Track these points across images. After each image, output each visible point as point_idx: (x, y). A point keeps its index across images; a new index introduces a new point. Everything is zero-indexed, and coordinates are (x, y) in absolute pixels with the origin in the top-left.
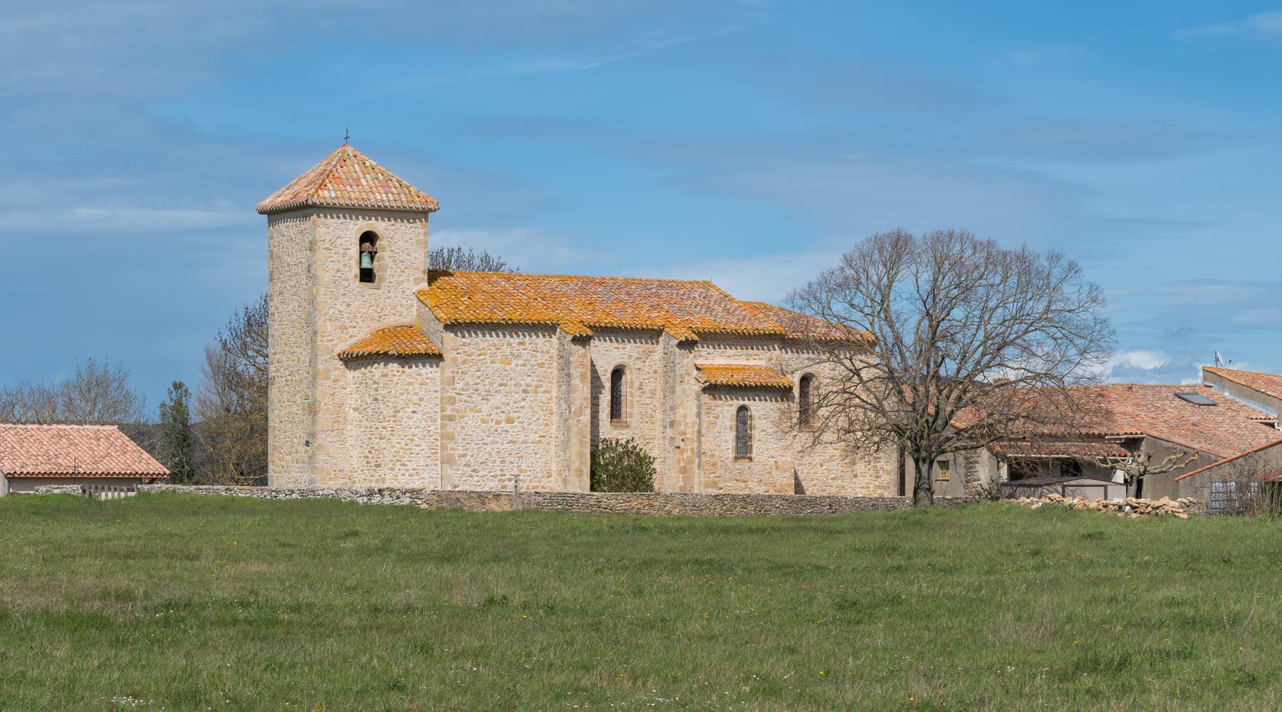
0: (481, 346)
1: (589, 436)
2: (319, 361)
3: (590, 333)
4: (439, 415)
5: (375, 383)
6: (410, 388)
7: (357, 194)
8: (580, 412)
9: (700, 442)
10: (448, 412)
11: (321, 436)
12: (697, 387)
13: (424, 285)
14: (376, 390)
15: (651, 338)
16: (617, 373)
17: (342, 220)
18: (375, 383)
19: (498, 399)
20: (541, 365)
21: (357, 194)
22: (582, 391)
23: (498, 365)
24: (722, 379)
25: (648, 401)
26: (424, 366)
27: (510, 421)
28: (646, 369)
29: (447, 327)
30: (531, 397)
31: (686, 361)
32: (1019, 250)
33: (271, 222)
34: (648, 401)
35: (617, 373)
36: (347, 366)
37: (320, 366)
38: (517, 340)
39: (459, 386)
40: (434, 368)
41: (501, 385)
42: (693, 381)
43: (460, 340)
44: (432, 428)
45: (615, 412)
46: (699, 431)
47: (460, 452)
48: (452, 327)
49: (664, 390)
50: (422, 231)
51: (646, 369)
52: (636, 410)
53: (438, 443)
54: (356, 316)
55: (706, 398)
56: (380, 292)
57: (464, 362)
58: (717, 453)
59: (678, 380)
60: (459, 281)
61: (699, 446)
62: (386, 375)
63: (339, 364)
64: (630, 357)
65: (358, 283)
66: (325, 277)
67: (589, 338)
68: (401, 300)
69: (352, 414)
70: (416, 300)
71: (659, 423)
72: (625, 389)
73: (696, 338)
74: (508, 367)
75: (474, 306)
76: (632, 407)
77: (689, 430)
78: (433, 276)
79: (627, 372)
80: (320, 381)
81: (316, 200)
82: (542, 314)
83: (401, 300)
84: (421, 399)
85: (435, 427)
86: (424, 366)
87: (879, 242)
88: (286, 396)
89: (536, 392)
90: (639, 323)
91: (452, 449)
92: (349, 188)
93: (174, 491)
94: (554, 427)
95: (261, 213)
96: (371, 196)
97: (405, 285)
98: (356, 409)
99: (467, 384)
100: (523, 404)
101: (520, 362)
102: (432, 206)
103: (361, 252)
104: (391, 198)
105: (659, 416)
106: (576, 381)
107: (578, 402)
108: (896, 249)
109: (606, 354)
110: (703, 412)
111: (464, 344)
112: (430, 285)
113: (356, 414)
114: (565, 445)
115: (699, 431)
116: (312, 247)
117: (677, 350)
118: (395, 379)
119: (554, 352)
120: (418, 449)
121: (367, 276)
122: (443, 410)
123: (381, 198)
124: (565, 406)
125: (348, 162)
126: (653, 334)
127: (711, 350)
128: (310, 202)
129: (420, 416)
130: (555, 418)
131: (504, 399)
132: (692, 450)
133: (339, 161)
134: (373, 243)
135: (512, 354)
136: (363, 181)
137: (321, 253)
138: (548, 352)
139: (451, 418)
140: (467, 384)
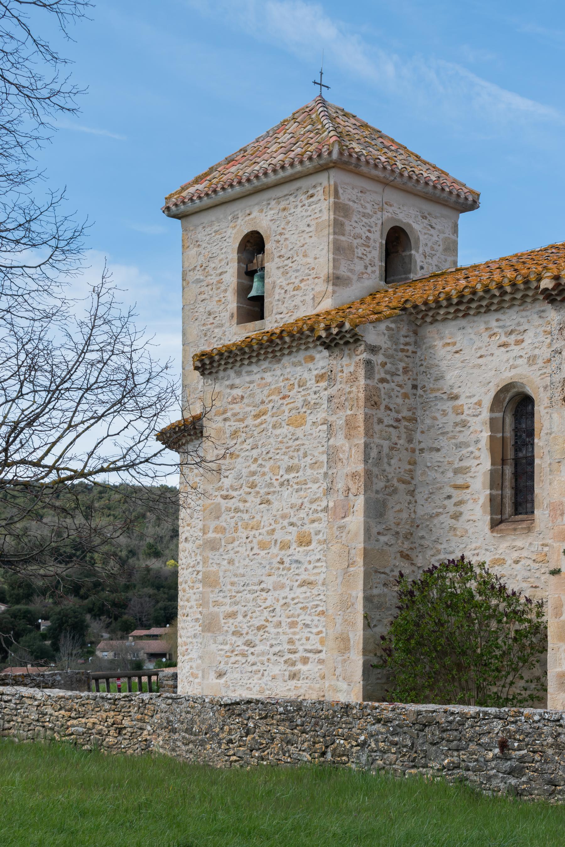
16: (517, 407)
41: (289, 469)
45: (515, 496)
65: (507, 376)
74: (299, 432)
135: (306, 403)
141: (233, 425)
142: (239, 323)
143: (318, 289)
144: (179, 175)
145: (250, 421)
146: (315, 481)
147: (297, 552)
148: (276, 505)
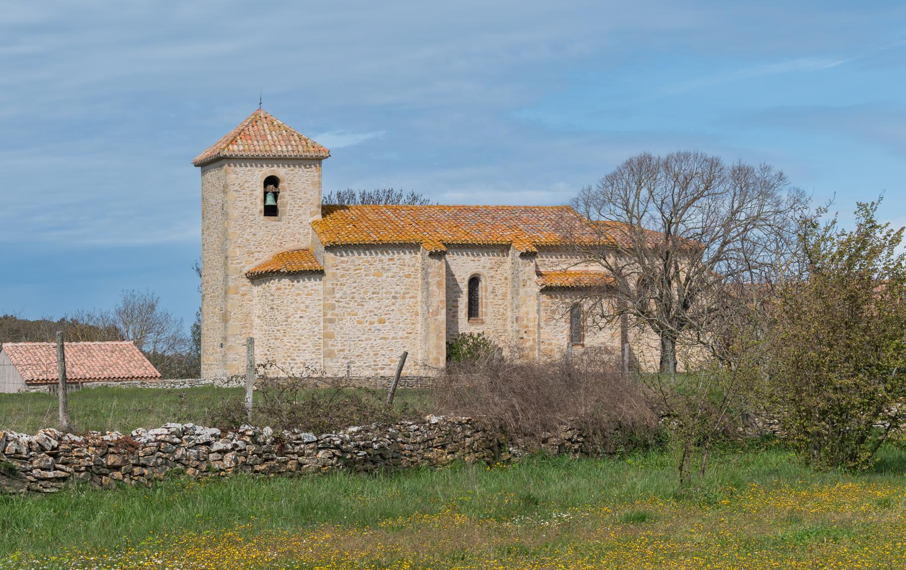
0: (357, 263)
1: (444, 332)
2: (230, 280)
3: (444, 249)
4: (322, 319)
5: (272, 295)
6: (299, 298)
7: (262, 147)
8: (437, 313)
9: (539, 333)
10: (329, 316)
11: (231, 339)
12: (537, 290)
13: (319, 217)
14: (273, 301)
15: (502, 251)
16: (474, 281)
17: (249, 167)
18: (272, 295)
19: (372, 304)
20: (408, 276)
21: (262, 147)
22: (439, 295)
23: (372, 277)
24: (557, 282)
25: (500, 302)
26: (310, 280)
27: (382, 321)
28: (498, 277)
29: (327, 248)
30: (399, 301)
31: (527, 269)
32: (736, 164)
33: (203, 173)
34: (500, 302)
35: (474, 281)
36: (253, 283)
37: (231, 284)
38: (388, 257)
39: (338, 295)
40: (318, 282)
41: (373, 293)
42: (534, 285)
43: (338, 258)
44: (316, 329)
45: (473, 310)
46: (539, 325)
47: (340, 348)
48: (332, 248)
49: (512, 293)
50: (316, 174)
51: (498, 277)
52: (490, 309)
53: (321, 341)
54: (264, 242)
55: (544, 298)
56: (281, 223)
57: (342, 276)
58: (553, 342)
59: (521, 284)
60: (352, 214)
61: (539, 337)
62: (280, 289)
63: (246, 281)
64: (484, 267)
65: (262, 217)
66: (234, 213)
67: (445, 253)
68: (298, 228)
69: (257, 321)
70: (311, 231)
71: (509, 319)
72: (481, 293)
73: (535, 250)
74: (379, 279)
75: (357, 229)
76: (486, 307)
77: (531, 324)
78: (327, 210)
79: (482, 279)
80: (230, 296)
81: (226, 153)
82: (411, 235)
83: (298, 228)
84: (307, 307)
85: (319, 329)
86: (310, 280)
87: (629, 163)
88: (211, 308)
89: (404, 298)
90: (492, 240)
91: (333, 345)
92: (255, 143)
93: (106, 386)
94: (419, 326)
95: (197, 165)
96: (273, 148)
97: (303, 217)
98: (259, 317)
99: (345, 293)
100: (392, 308)
101: (390, 274)
102: (324, 154)
103: (266, 193)
104: (290, 148)
105: (509, 313)
106: (433, 288)
107: (435, 304)
108: (642, 169)
109: (464, 266)
110: (541, 309)
111: (342, 262)
112: (324, 215)
113: (259, 321)
114: (426, 339)
115: (539, 325)
116: (225, 190)
117: (520, 260)
118: (287, 291)
119: (419, 266)
120: (304, 347)
121: (271, 211)
122: (325, 315)
123: (282, 149)
124: (425, 308)
125: (259, 123)
126: (504, 248)
127: (554, 259)
128: (221, 155)
129: (306, 320)
130: (420, 318)
131: (377, 305)
132: (534, 340)
133: (251, 122)
134: (276, 185)
135: (383, 268)
136: (269, 137)
137: (232, 195)
138: (414, 266)
139: (331, 321)
140: (345, 293)
141: (343, 272)
142: (265, 215)
143: (312, 209)
144: (203, 154)
145: (351, 271)
146: (387, 299)
147: (379, 326)
148: (366, 306)
